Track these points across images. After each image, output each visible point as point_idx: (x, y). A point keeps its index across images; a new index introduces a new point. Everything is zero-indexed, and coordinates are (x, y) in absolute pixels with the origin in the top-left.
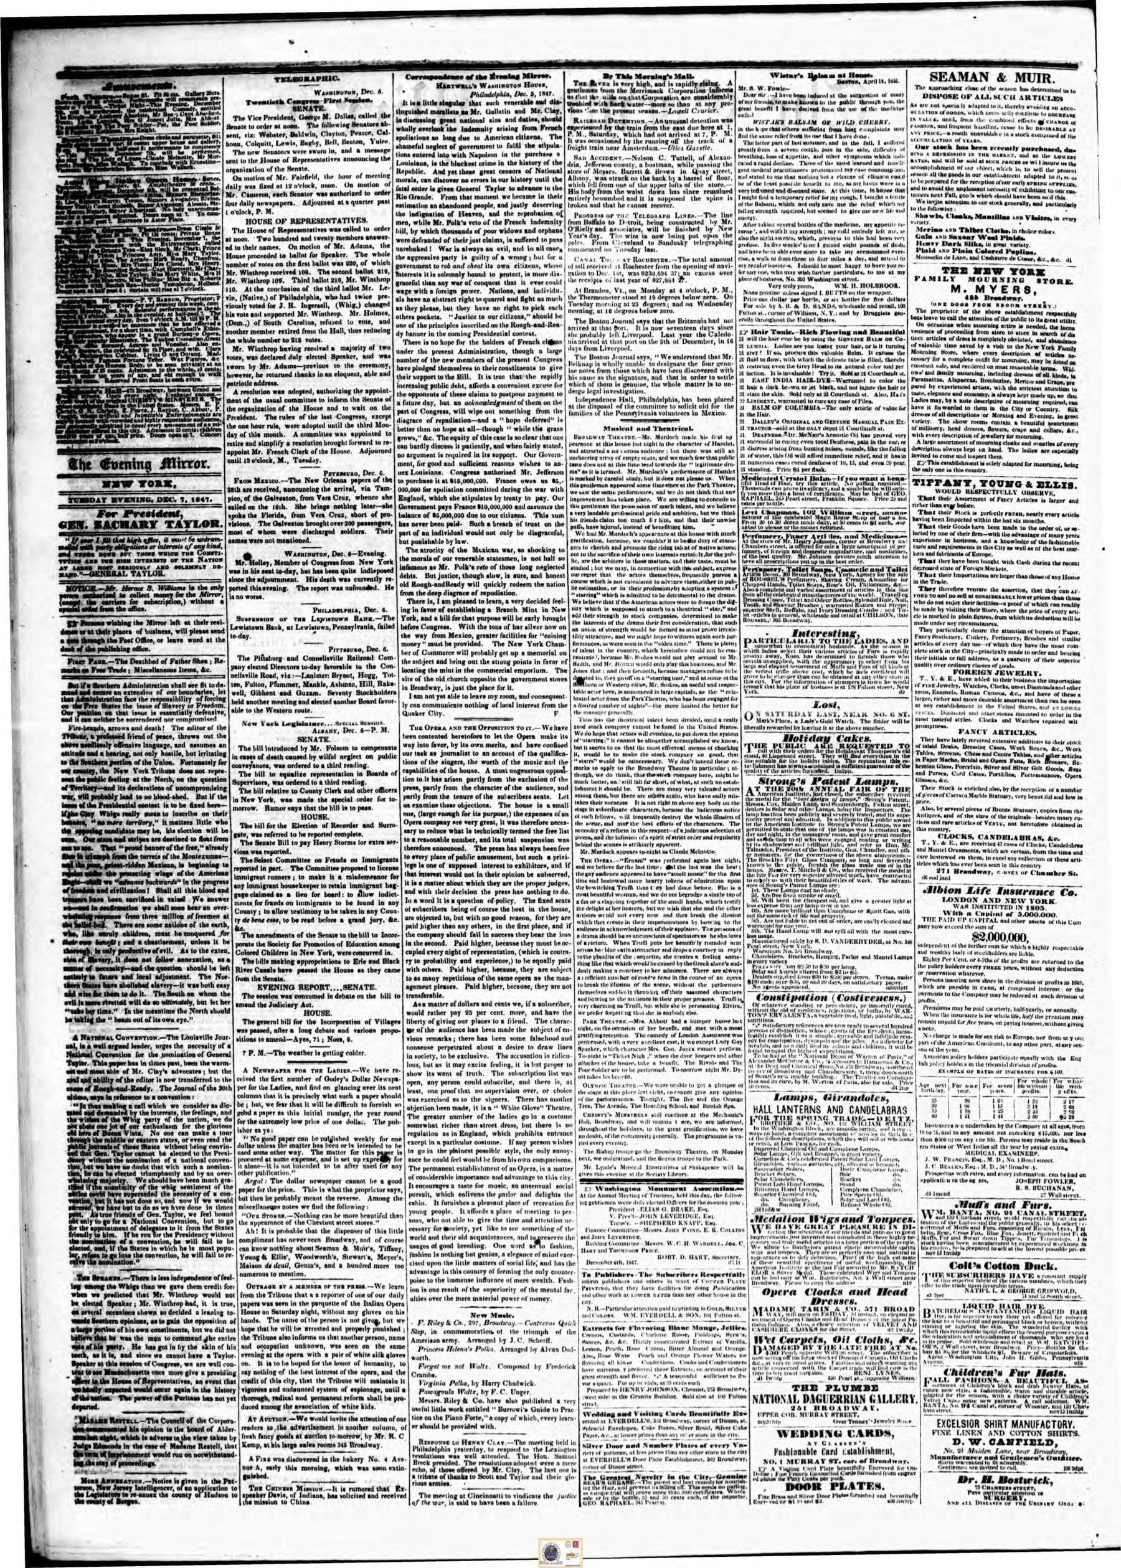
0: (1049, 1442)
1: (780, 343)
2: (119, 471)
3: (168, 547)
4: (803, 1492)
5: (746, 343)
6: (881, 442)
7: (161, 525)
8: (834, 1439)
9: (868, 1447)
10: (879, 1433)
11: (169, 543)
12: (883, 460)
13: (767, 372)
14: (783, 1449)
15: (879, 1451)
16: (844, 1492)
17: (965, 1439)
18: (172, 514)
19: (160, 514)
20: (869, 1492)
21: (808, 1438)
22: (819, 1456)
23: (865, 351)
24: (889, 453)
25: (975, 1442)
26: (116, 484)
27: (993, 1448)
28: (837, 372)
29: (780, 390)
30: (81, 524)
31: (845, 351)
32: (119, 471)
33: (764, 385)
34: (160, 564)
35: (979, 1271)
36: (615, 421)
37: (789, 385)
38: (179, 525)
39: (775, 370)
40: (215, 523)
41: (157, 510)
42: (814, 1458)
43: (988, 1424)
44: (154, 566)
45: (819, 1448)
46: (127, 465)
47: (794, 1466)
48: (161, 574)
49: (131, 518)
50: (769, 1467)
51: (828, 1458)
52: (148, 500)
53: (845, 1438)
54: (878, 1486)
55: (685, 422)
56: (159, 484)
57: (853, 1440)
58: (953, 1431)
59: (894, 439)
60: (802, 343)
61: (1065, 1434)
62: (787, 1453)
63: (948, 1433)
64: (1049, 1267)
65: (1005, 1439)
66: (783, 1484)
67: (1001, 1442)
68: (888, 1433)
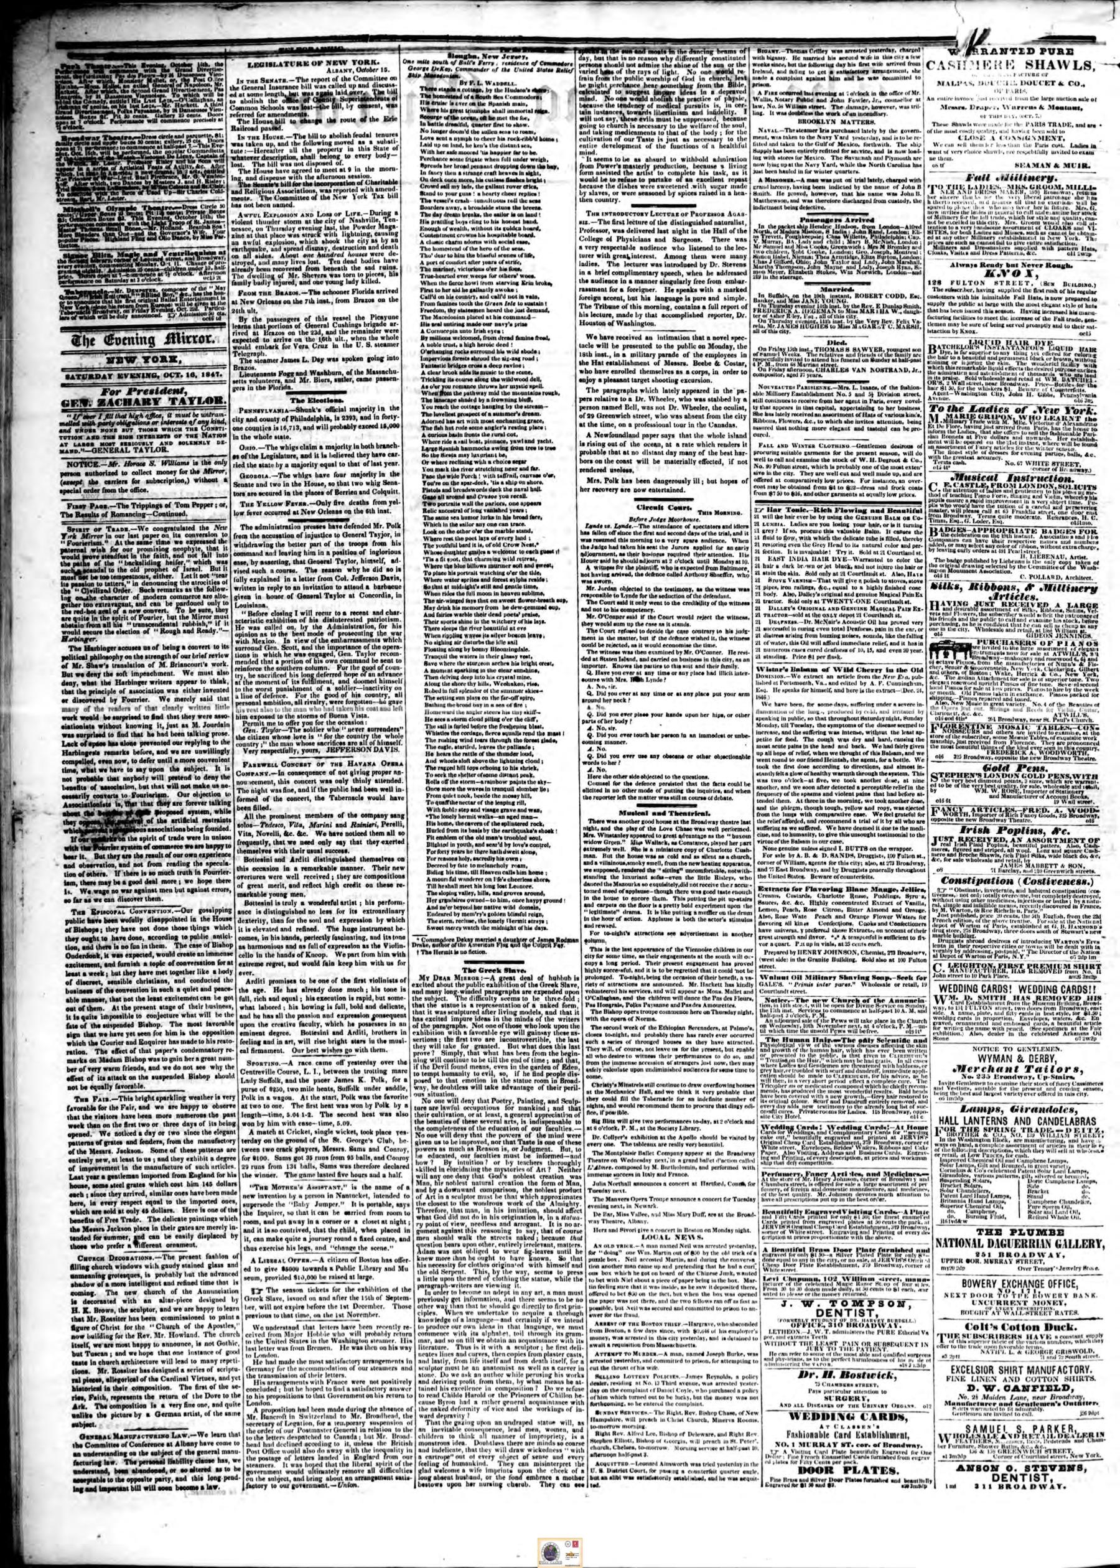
0: (1066, 1387)
1: (795, 521)
2: (121, 347)
3: (172, 423)
4: (815, 1475)
5: (761, 520)
6: (898, 629)
7: (165, 401)
8: (846, 1422)
9: (882, 1430)
10: (893, 1417)
11: (173, 418)
12: (900, 647)
13: (784, 551)
14: (796, 1431)
15: (893, 1436)
16: (857, 1476)
17: (979, 1385)
18: (176, 391)
19: (164, 391)
20: (884, 1477)
21: (820, 1422)
22: (831, 1439)
23: (883, 530)
24: (906, 640)
25: (989, 1388)
26: (120, 360)
27: (1008, 1395)
28: (856, 551)
29: (796, 570)
30: (85, 401)
31: (862, 529)
32: (121, 347)
33: (780, 563)
34: (164, 440)
35: (995, 1332)
36: (630, 806)
37: (804, 563)
38: (183, 401)
39: (792, 549)
40: (219, 400)
41: (161, 388)
42: (826, 1441)
43: (1002, 1370)
44: (157, 443)
45: (831, 1431)
46: (131, 341)
47: (806, 1449)
48: (164, 450)
49: (134, 396)
50: (781, 1449)
51: (840, 1441)
52: (155, 376)
53: (858, 1421)
54: (893, 1471)
55: (702, 806)
56: (164, 359)
57: (866, 1423)
58: (968, 1377)
59: (911, 626)
60: (817, 521)
61: (1081, 1380)
62: (800, 1435)
63: (962, 1379)
64: (1069, 1328)
65: (1020, 1385)
66: (796, 1468)
67: (1016, 1389)
68: (902, 1418)
